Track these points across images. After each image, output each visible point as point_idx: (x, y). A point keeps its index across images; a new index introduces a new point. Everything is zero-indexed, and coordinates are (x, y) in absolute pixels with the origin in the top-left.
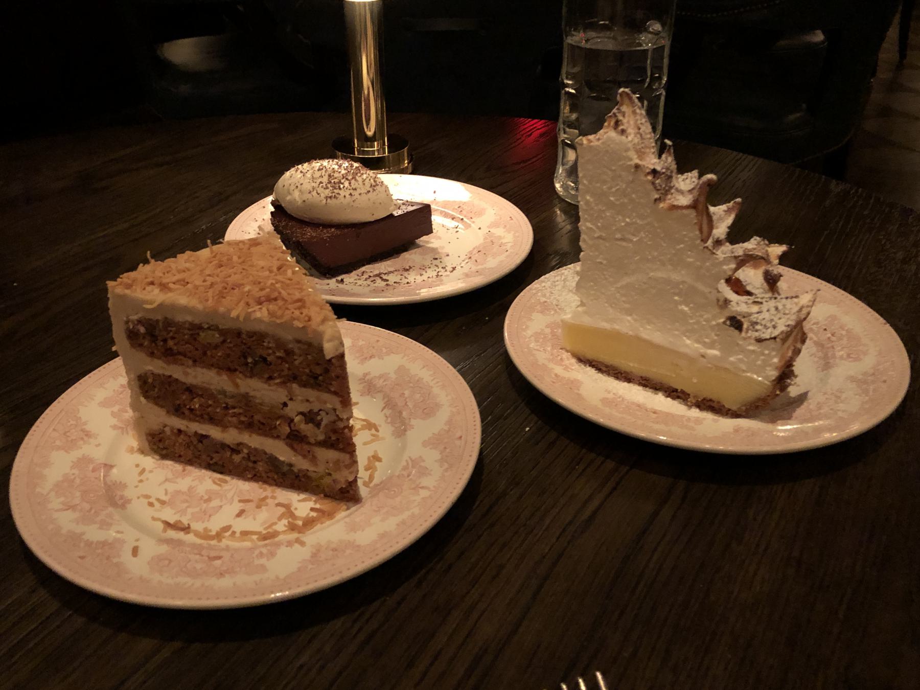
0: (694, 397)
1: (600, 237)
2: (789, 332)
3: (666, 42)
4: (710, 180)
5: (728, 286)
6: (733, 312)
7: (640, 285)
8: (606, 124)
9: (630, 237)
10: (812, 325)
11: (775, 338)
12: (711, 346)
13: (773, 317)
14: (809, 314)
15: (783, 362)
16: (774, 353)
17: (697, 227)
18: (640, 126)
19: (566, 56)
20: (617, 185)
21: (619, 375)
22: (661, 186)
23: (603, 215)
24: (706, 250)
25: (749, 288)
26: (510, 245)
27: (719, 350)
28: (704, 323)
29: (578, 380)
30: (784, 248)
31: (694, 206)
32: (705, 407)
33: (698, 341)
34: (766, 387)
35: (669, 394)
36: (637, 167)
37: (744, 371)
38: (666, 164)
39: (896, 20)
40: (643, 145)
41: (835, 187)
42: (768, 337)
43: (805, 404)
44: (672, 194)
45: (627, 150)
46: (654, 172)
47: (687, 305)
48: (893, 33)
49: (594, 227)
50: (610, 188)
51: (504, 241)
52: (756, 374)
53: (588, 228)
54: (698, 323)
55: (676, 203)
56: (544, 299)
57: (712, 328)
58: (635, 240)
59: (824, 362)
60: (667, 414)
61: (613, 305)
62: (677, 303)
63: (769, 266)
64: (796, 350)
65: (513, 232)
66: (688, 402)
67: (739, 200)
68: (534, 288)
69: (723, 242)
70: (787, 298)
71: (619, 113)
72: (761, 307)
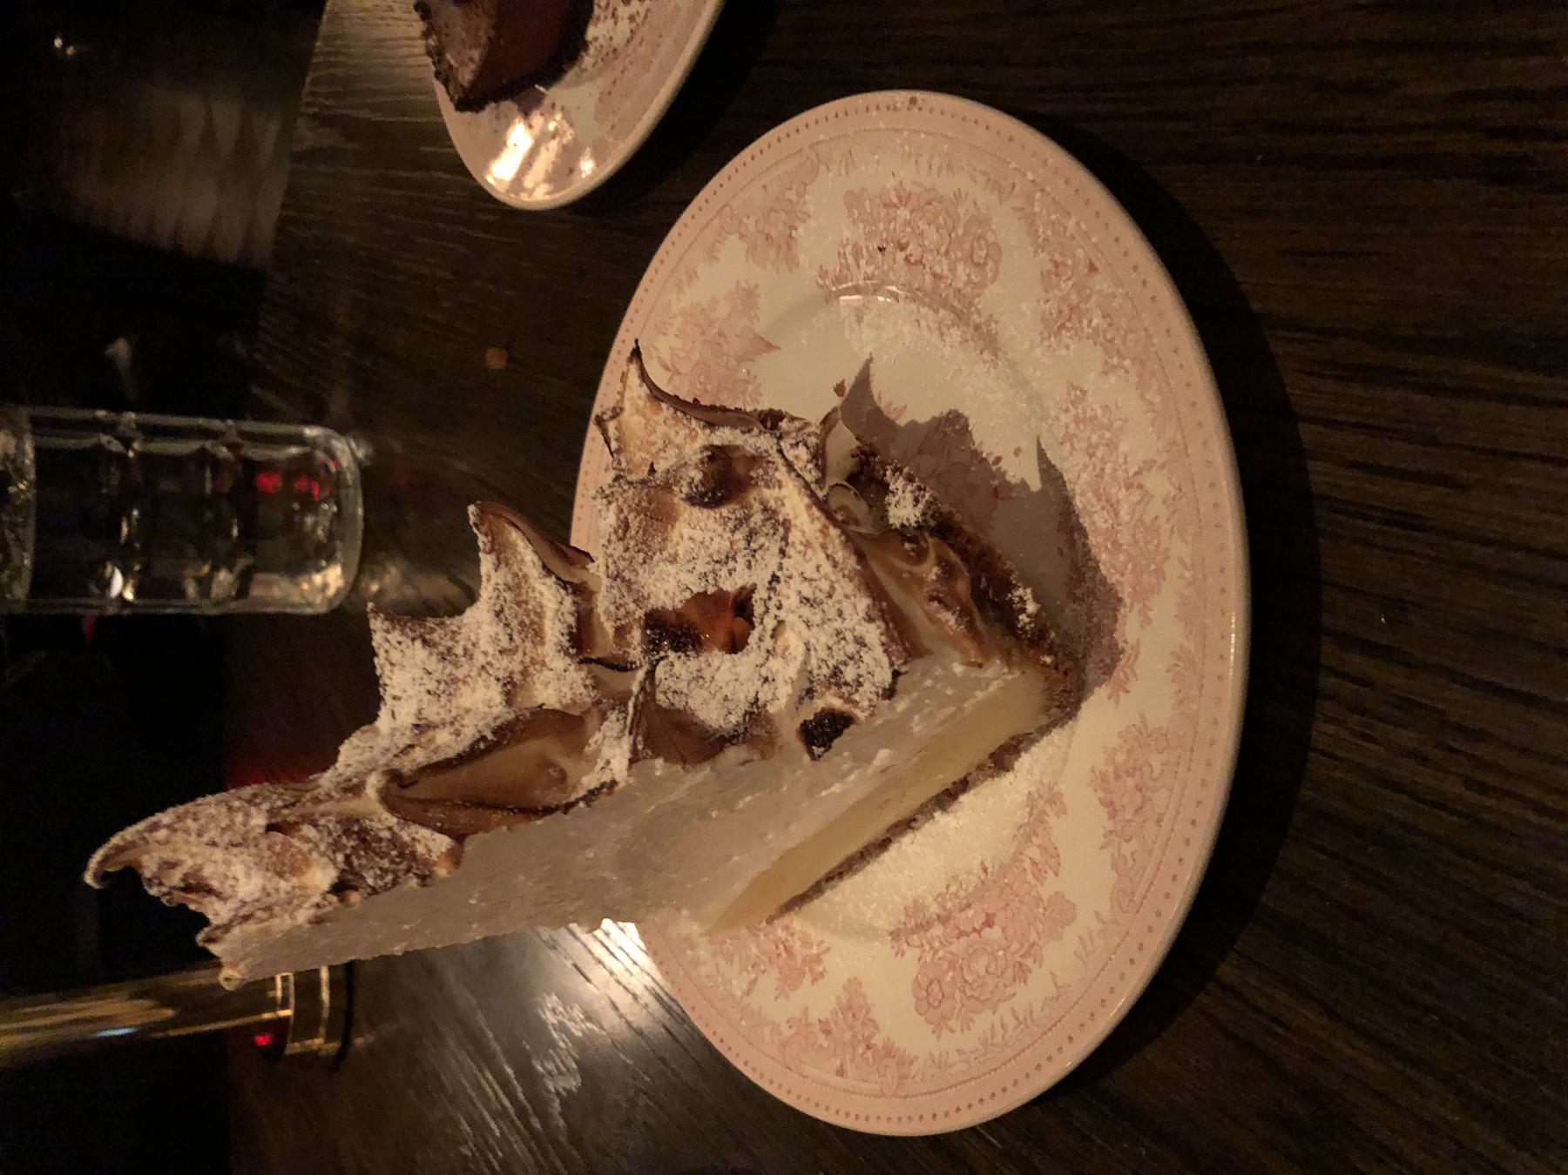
18: (206, 839)
19: (73, 441)
44: (414, 839)
63: (676, 489)
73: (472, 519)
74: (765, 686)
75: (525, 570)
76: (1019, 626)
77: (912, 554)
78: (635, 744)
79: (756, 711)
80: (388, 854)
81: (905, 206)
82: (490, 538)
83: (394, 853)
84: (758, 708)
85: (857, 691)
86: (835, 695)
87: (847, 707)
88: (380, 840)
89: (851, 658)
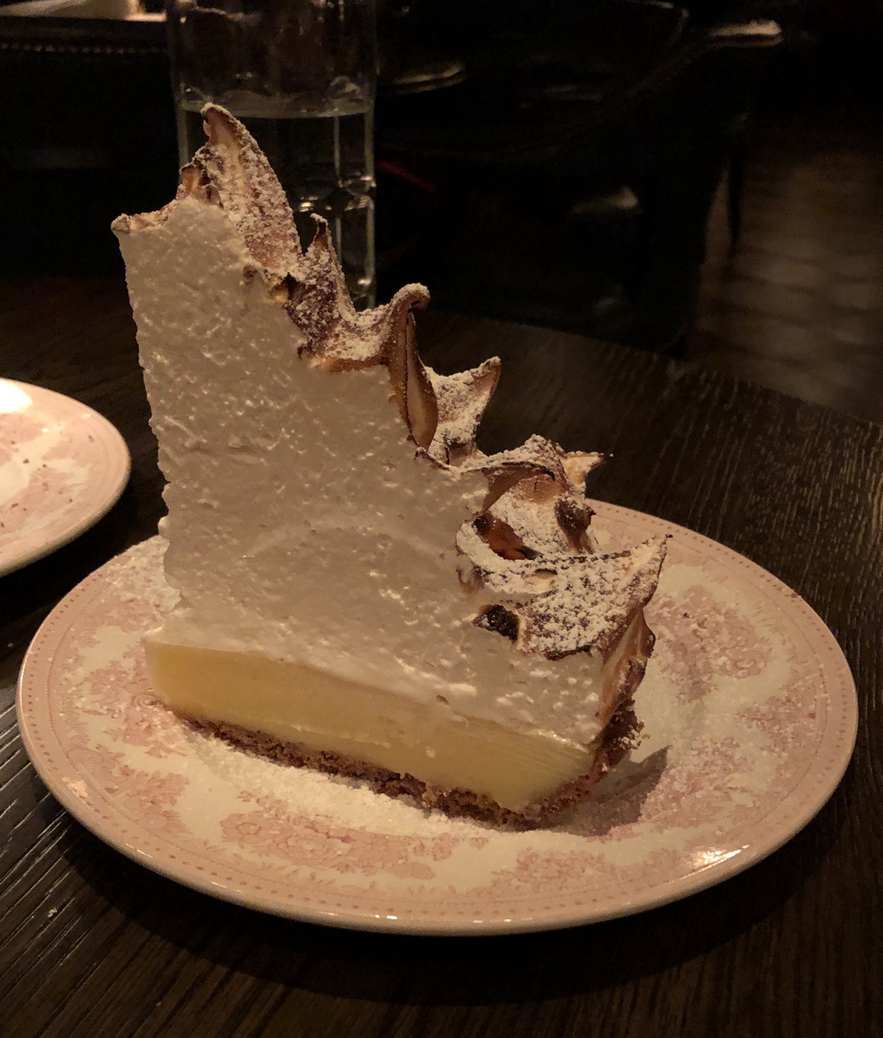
0: (434, 789)
1: (197, 448)
2: (615, 631)
3: (367, 109)
4: (414, 298)
5: (484, 542)
6: (495, 596)
7: (296, 550)
8: (181, 187)
9: (260, 441)
10: (661, 608)
11: (586, 649)
12: (457, 674)
13: (578, 601)
14: (654, 588)
15: (610, 700)
16: (588, 682)
17: (396, 408)
18: (259, 188)
20: (216, 321)
21: (277, 751)
22: (309, 317)
23: (196, 396)
24: (420, 459)
25: (528, 542)
26: (77, 490)
27: (474, 682)
28: (437, 625)
29: (179, 776)
30: (594, 458)
31: (383, 359)
32: (458, 808)
33: (427, 666)
34: (579, 757)
35: (383, 786)
36: (250, 273)
37: (530, 725)
38: (316, 268)
39: (721, 193)
40: (267, 231)
41: (675, 371)
42: (573, 647)
43: (664, 780)
44: (337, 336)
45: (225, 235)
46: (290, 284)
47: (397, 589)
48: (719, 210)
49: (182, 427)
50: (201, 331)
51: (68, 482)
52: (556, 730)
53: (168, 428)
54: (424, 625)
55: (344, 356)
56: (129, 595)
57: (455, 634)
58: (270, 448)
59: (690, 682)
60: (377, 839)
61: (247, 599)
62: (375, 584)
63: (567, 493)
64: (634, 669)
65: (89, 465)
66: (423, 800)
67: (496, 359)
68: (109, 572)
69: (468, 448)
70: (606, 557)
71: (206, 160)
72: (553, 582)
73: (492, 360)
74: (500, 578)
75: (471, 403)
76: (619, 739)
77: (648, 642)
78: (497, 469)
79: (482, 575)
80: (322, 319)
81: (726, 618)
82: (482, 375)
83: (324, 322)
84: (484, 576)
85: (540, 636)
86: (528, 622)
87: (521, 632)
88: (330, 311)
89: (564, 622)
